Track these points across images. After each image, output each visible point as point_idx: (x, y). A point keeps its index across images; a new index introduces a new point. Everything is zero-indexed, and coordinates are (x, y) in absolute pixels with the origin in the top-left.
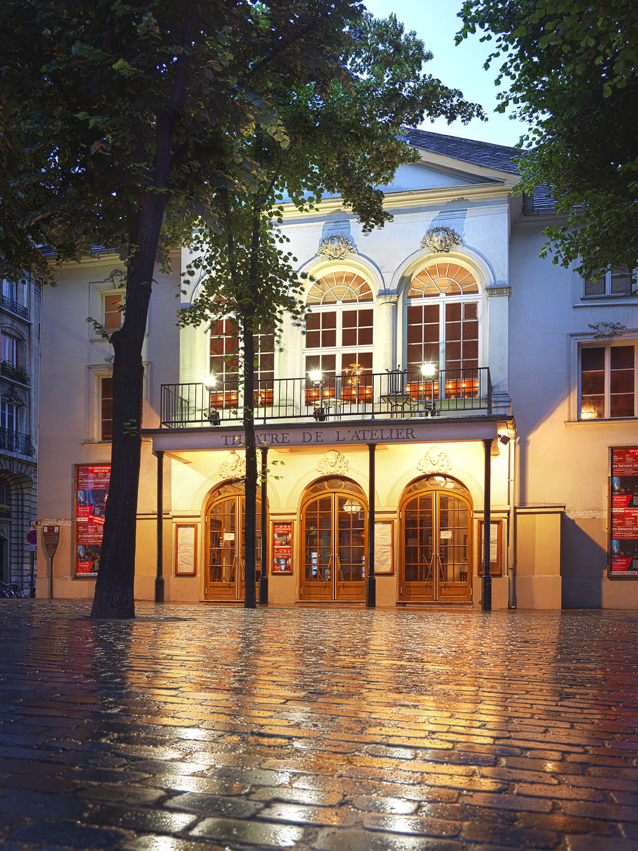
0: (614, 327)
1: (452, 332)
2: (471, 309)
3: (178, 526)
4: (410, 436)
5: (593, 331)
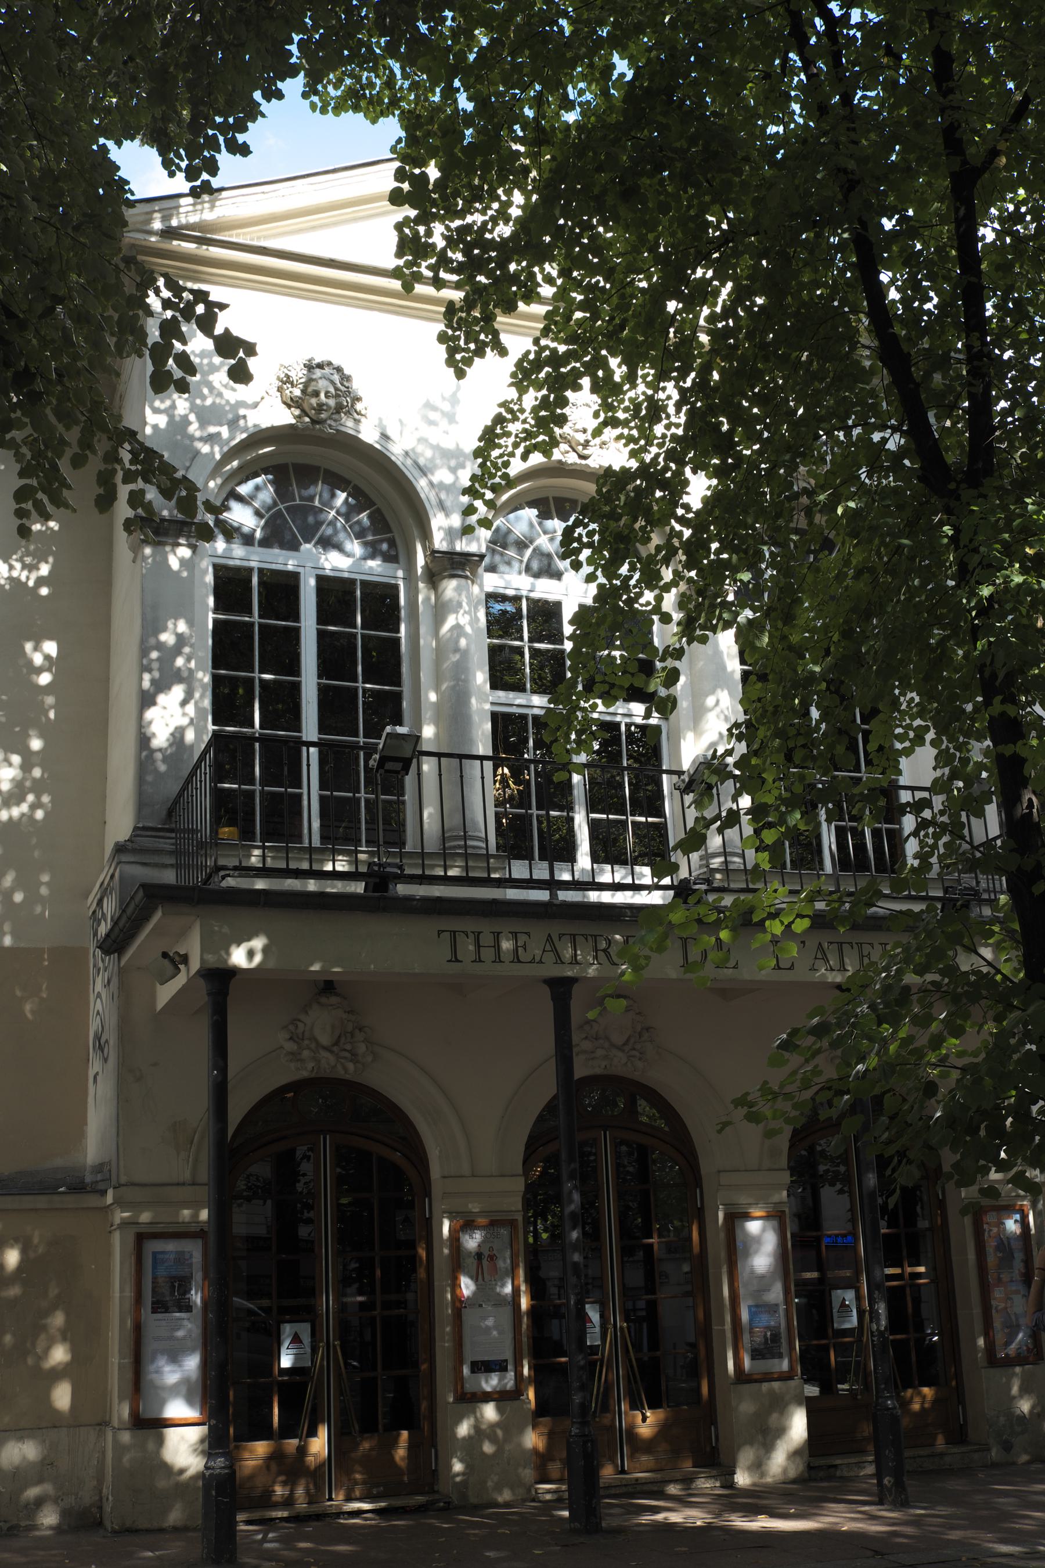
1: (334, 657)
2: (382, 604)
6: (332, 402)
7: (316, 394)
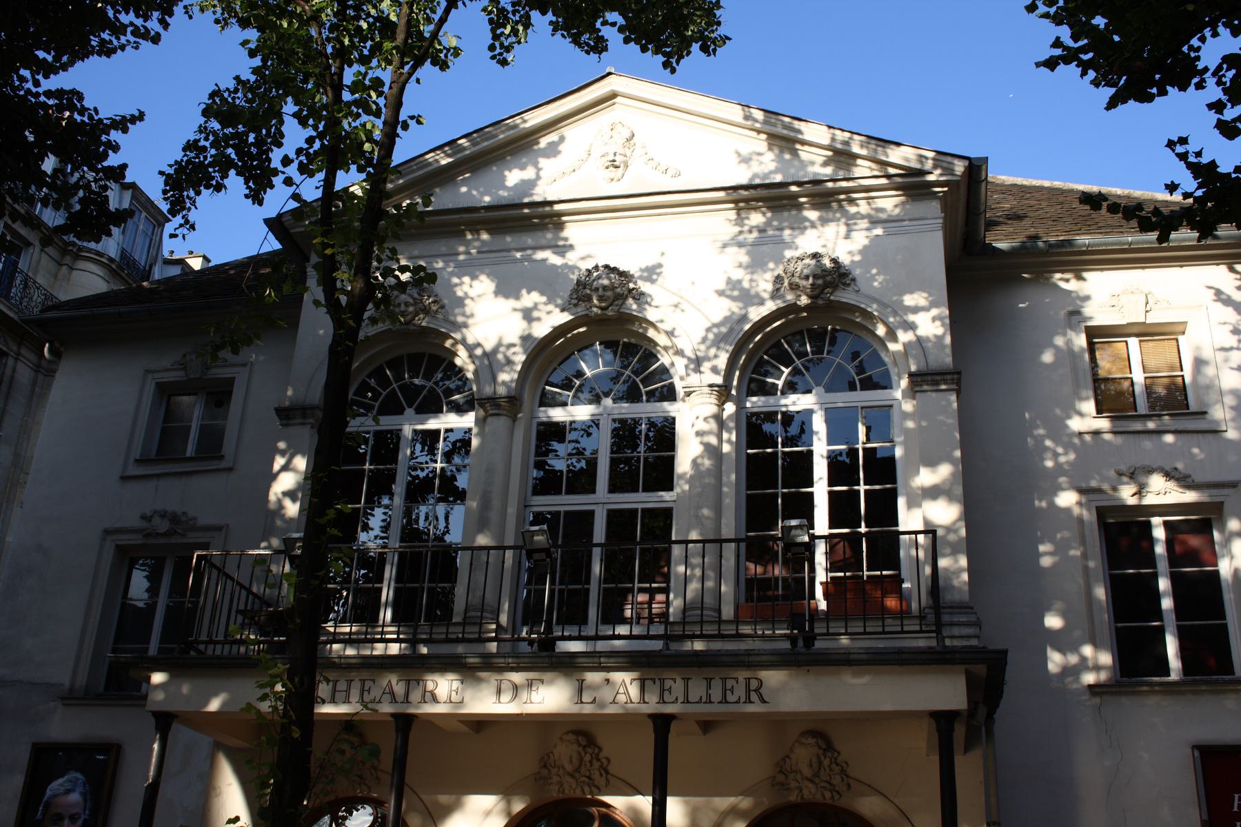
0: (175, 519)
4: (754, 697)
5: (144, 524)
7: (399, 305)
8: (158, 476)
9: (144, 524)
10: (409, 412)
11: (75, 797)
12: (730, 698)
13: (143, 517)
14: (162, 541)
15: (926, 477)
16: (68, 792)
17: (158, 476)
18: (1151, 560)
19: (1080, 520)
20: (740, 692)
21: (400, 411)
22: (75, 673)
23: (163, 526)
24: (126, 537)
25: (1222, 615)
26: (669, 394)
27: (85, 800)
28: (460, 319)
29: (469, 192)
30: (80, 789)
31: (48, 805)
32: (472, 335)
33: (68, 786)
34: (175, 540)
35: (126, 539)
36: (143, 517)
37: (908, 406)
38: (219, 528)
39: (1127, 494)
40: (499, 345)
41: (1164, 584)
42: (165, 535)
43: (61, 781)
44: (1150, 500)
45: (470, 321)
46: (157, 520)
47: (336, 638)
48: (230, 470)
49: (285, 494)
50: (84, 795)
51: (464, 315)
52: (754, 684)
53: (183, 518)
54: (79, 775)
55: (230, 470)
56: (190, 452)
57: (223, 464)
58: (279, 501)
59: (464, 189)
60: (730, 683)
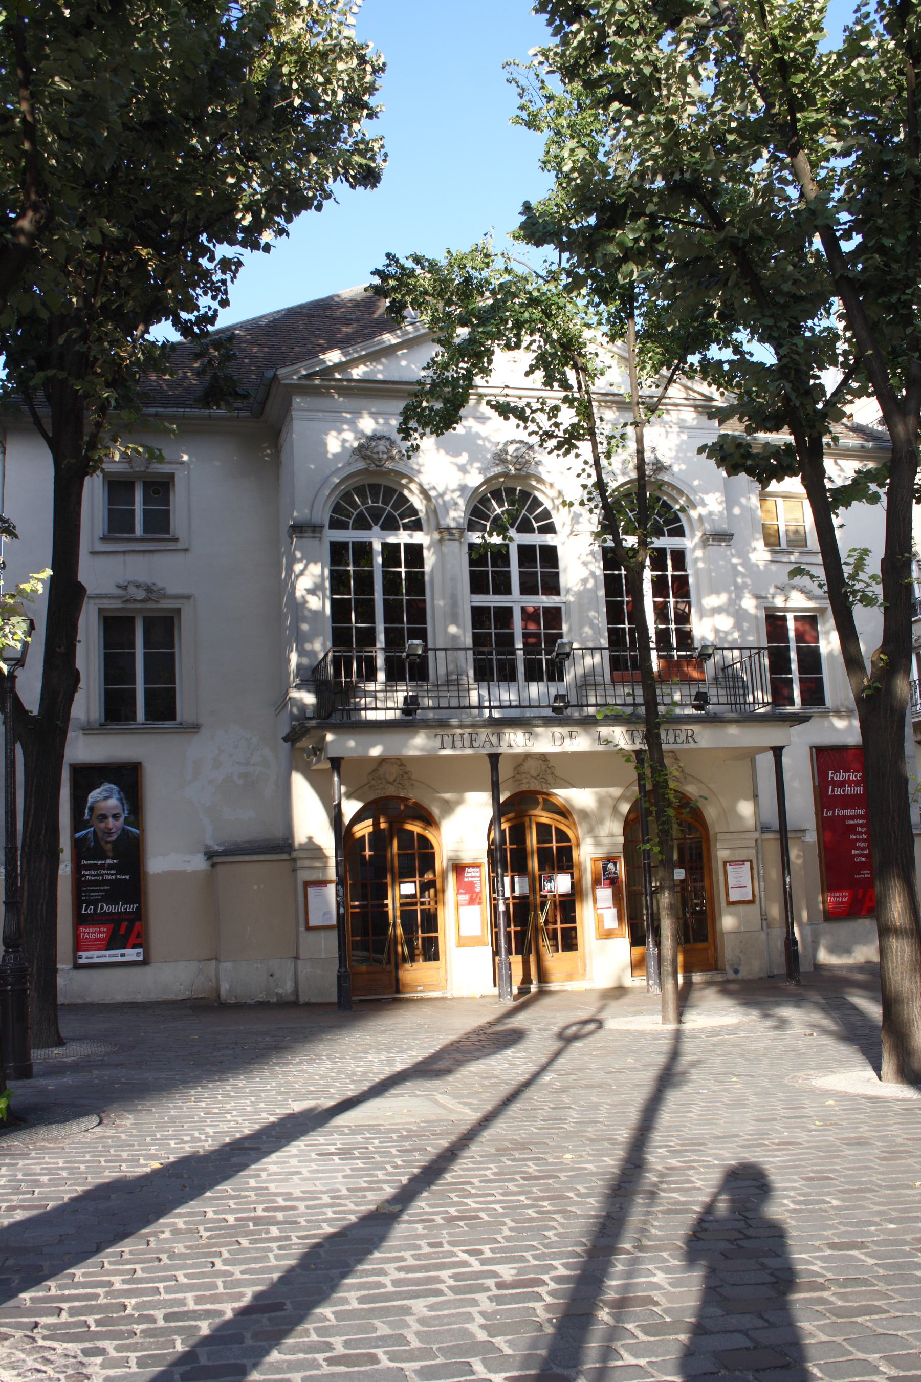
0: (149, 590)
3: (751, 861)
5: (120, 592)
6: (385, 456)
8: (124, 552)
9: (120, 592)
10: (376, 529)
11: (113, 802)
12: (679, 741)
13: (119, 587)
14: (139, 606)
15: (710, 601)
16: (107, 798)
17: (144, 551)
18: (786, 639)
19: (756, 617)
20: (683, 737)
21: (369, 528)
22: (88, 710)
23: (141, 594)
24: (106, 601)
25: (820, 671)
26: (549, 529)
27: (123, 804)
28: (416, 467)
29: (408, 366)
30: (116, 796)
31: (92, 809)
32: (425, 479)
33: (105, 794)
34: (150, 605)
35: (107, 604)
36: (119, 587)
37: (699, 553)
38: (188, 597)
39: (779, 602)
40: (447, 489)
41: (793, 655)
42: (142, 601)
43: (98, 791)
44: (790, 604)
45: (422, 469)
46: (132, 590)
47: (857, 783)
48: (186, 550)
49: (309, 592)
50: (120, 800)
51: (418, 464)
52: (690, 733)
53: (155, 588)
54: (112, 786)
55: (186, 550)
56: (139, 530)
57: (179, 546)
58: (303, 597)
59: (404, 363)
60: (678, 732)
